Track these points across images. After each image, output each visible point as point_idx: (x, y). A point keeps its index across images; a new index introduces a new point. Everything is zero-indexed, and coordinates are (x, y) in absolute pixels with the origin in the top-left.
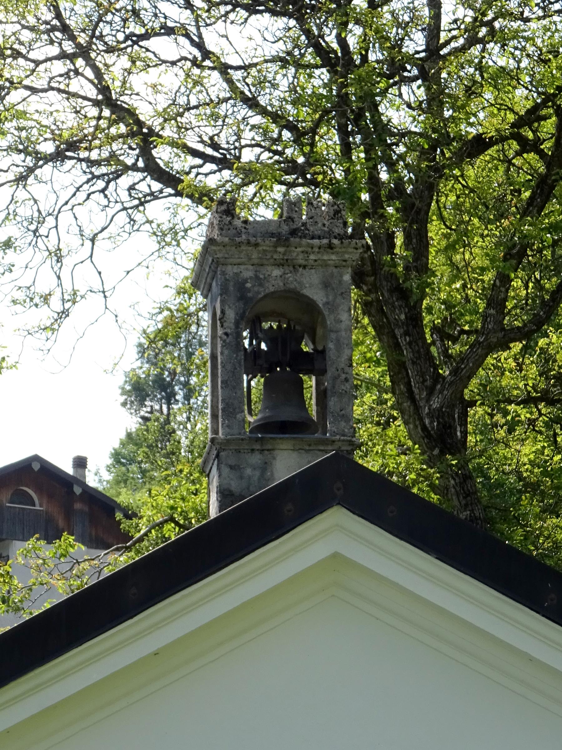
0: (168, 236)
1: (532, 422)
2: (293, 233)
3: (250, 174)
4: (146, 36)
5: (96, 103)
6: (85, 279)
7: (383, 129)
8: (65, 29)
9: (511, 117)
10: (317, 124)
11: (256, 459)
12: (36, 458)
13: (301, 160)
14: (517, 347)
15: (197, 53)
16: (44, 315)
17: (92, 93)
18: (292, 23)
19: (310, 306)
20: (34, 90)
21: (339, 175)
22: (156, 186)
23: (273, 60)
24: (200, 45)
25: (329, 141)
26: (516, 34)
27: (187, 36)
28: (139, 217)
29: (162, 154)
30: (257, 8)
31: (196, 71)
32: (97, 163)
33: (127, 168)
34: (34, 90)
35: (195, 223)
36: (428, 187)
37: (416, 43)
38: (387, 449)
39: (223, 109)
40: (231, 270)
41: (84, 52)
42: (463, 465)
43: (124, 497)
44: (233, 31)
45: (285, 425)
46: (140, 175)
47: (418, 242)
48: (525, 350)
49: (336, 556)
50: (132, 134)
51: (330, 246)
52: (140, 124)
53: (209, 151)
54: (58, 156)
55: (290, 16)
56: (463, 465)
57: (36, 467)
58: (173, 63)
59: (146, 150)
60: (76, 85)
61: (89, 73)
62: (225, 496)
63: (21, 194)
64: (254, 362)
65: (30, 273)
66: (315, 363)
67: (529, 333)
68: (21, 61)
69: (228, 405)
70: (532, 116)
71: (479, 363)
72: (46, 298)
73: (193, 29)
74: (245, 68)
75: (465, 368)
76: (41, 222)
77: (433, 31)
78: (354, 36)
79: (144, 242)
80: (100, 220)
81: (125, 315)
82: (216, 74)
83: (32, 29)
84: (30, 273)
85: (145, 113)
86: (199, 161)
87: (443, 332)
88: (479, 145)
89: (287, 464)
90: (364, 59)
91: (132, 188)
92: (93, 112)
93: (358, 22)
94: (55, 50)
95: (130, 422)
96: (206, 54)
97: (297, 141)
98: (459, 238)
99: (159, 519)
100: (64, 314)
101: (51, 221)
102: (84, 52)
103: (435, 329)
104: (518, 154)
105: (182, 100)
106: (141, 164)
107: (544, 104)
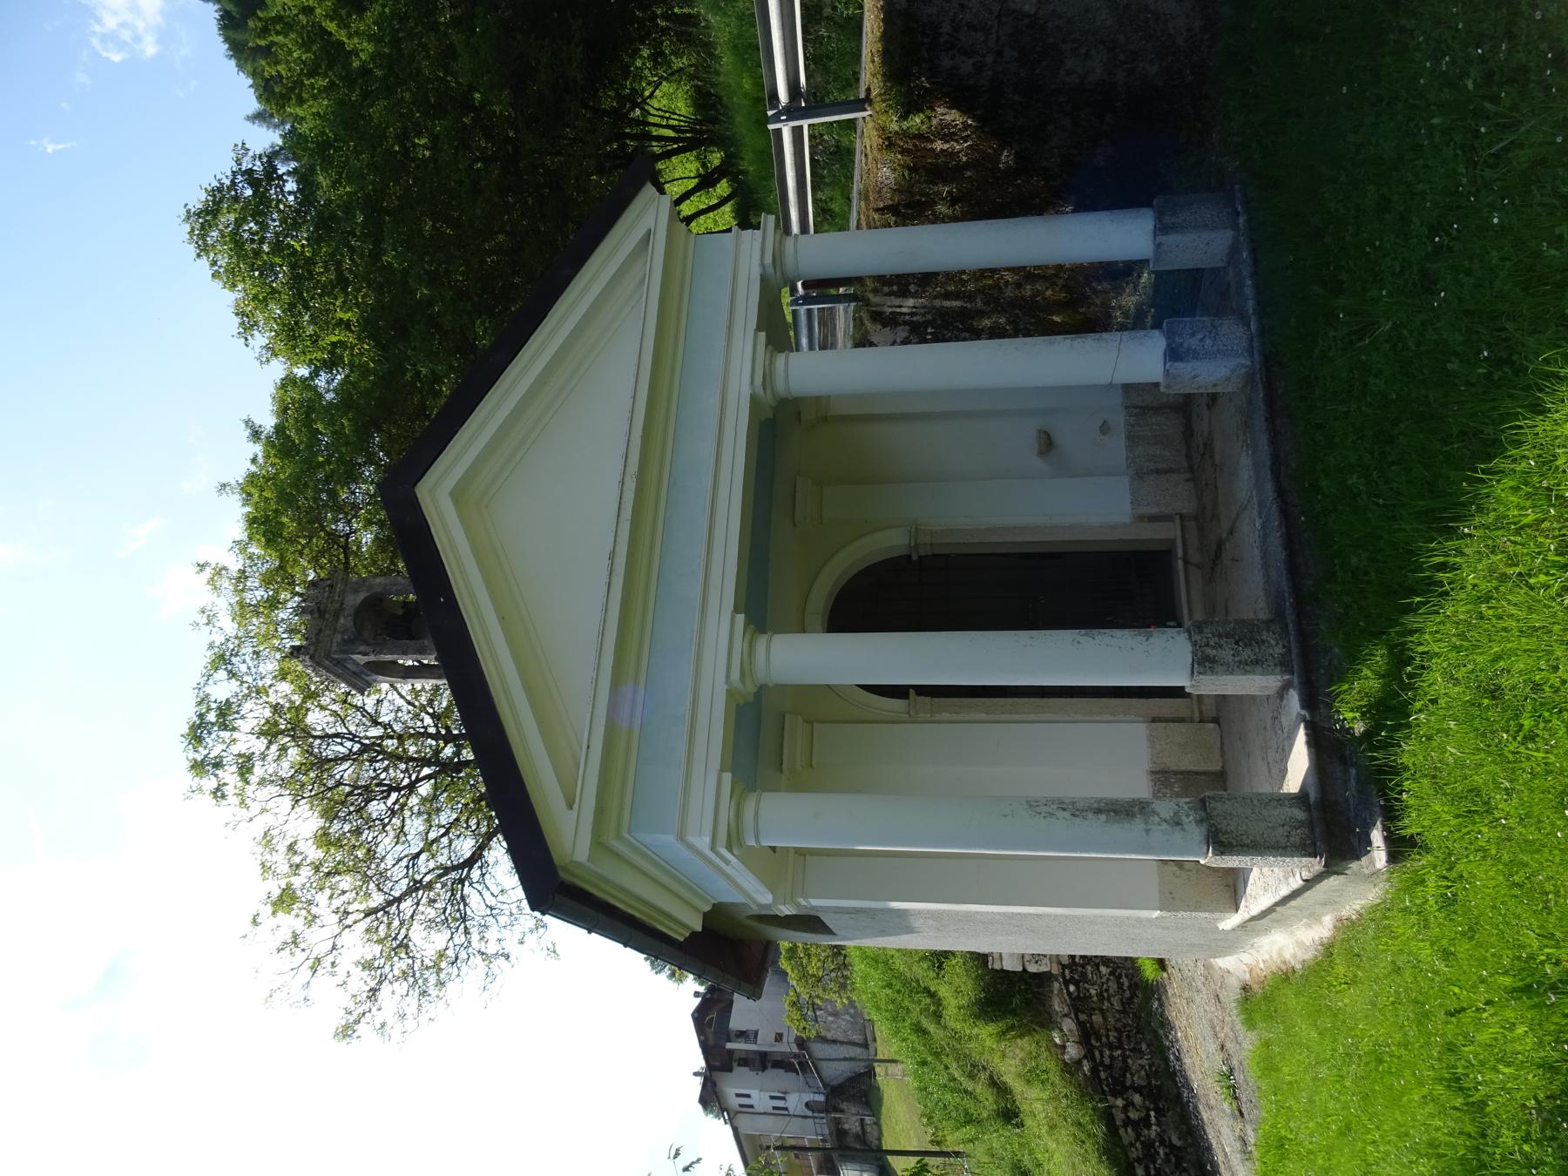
49: (451, 494)
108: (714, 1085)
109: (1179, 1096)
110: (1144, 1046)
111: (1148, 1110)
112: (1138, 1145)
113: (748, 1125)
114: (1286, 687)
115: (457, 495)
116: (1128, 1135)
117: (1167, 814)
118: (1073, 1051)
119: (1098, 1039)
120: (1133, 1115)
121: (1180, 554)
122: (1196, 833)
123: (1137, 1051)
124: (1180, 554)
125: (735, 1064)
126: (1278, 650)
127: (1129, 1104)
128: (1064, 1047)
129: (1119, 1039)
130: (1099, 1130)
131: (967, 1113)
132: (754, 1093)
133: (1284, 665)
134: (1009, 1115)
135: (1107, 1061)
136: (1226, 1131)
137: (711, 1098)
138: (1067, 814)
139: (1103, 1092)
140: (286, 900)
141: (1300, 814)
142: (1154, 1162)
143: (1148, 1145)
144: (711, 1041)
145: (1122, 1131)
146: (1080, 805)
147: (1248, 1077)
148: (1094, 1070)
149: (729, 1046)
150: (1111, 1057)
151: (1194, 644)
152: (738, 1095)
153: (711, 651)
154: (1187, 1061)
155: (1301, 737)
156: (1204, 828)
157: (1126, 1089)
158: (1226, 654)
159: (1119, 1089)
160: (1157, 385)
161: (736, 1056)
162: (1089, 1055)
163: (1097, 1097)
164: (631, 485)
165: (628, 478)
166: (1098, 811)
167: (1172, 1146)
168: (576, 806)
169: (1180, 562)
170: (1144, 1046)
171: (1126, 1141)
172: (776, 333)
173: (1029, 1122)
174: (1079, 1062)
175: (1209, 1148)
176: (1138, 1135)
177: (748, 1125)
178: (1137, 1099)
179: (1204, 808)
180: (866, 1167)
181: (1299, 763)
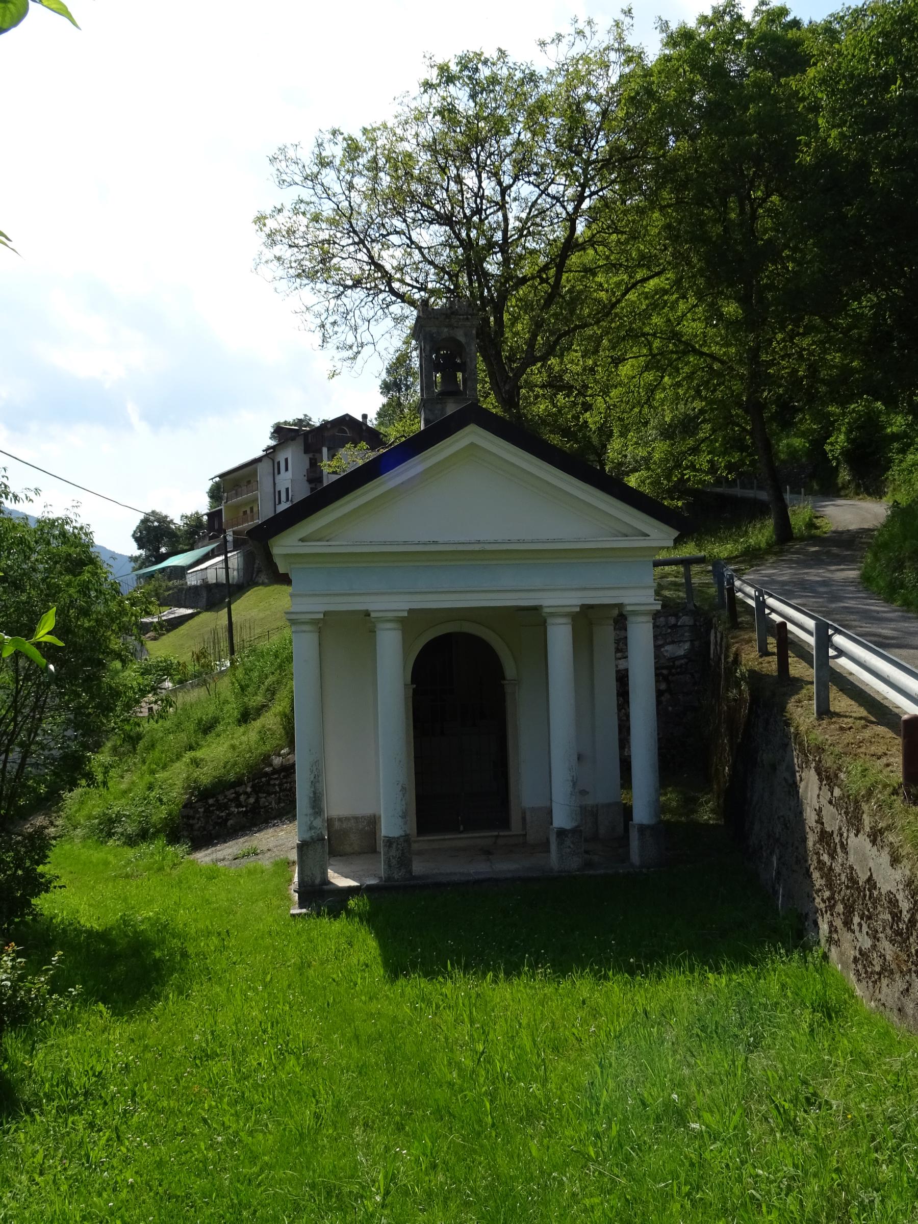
0: (399, 320)
1: (543, 395)
2: (452, 313)
3: (433, 292)
4: (388, 234)
5: (367, 263)
6: (366, 338)
7: (486, 274)
8: (355, 232)
9: (537, 268)
10: (459, 271)
11: (439, 406)
12: (347, 415)
13: (452, 287)
14: (539, 364)
15: (408, 242)
16: (350, 353)
17: (366, 259)
18: (448, 228)
19: (459, 344)
20: (343, 258)
21: (468, 293)
22: (394, 298)
23: (441, 245)
24: (410, 238)
25: (464, 279)
26: (539, 233)
27: (404, 234)
28: (386, 311)
29: (396, 285)
30: (62, 644)
31: (409, 250)
32: (370, 289)
33: (381, 291)
34: (343, 258)
35: (412, 313)
36: (504, 296)
37: (498, 236)
38: (491, 404)
39: (420, 265)
40: (428, 329)
41: (362, 242)
42: (518, 412)
43: (382, 430)
44: (423, 232)
45: (450, 392)
46: (386, 294)
47: (499, 321)
48: (542, 366)
49: (472, 444)
50: (383, 277)
51: (467, 319)
52: (387, 272)
53: (415, 284)
54: (355, 286)
55: (447, 225)
56: (518, 412)
57: (347, 418)
58: (399, 246)
59: (389, 284)
60: (360, 256)
61: (365, 250)
62: (427, 421)
63: (339, 302)
64: (437, 367)
65: (344, 335)
66: (462, 368)
67: (544, 358)
68: (336, 246)
69: (427, 385)
70: (546, 268)
71: (524, 372)
72: (351, 347)
73: (407, 232)
74: (429, 248)
75: (521, 371)
76: (348, 314)
77: (505, 231)
78: (474, 234)
79: (389, 322)
80: (372, 313)
81: (383, 353)
82: (417, 251)
83: (341, 232)
84: (344, 335)
85: (388, 267)
86: (410, 288)
87: (511, 359)
88: (524, 280)
89: (451, 408)
90: (477, 243)
91: (384, 299)
92: (367, 267)
93: (475, 228)
94: (351, 241)
95: (384, 400)
96: (412, 242)
97: (450, 279)
98: (515, 319)
99: (398, 435)
100: (359, 352)
101: (351, 314)
102: (362, 242)
103: (506, 357)
104: (540, 284)
105: (403, 262)
106: (387, 289)
107: (551, 262)
108: (293, 439)
109: (255, 825)
110: (282, 805)
111: (246, 807)
112: (226, 800)
113: (264, 470)
114: (381, 878)
115: (472, 445)
116: (231, 794)
117: (315, 824)
118: (277, 761)
119: (285, 777)
120: (242, 798)
121: (501, 834)
122: (307, 836)
123: (279, 801)
124: (501, 834)
125: (311, 455)
126: (396, 877)
127: (248, 795)
128: (279, 755)
129: (285, 790)
130: (232, 777)
131: (248, 686)
132: (289, 475)
133: (389, 879)
134: (245, 717)
135: (272, 782)
136: (230, 851)
137: (280, 431)
138: (312, 779)
139: (254, 780)
140: (353, 150)
141: (317, 881)
142: (217, 810)
143: (225, 807)
144: (326, 434)
145: (232, 791)
146: (317, 785)
147: (250, 863)
148: (266, 774)
149: (325, 450)
150: (274, 785)
151: (398, 838)
152: (286, 460)
153: (389, 601)
154: (271, 830)
155: (353, 883)
156: (308, 840)
157: (257, 794)
158: (393, 852)
159: (257, 789)
160: (552, 824)
161: (317, 455)
162: (275, 771)
163: (250, 776)
164: (477, 547)
165: (482, 545)
166: (315, 793)
167: (227, 820)
168: (301, 543)
169: (496, 833)
170: (282, 805)
171: (227, 793)
172: (586, 619)
173: (242, 729)
174: (271, 765)
175: (225, 842)
176: (231, 800)
177: (264, 470)
178: (252, 800)
179: (319, 840)
180: (241, 574)
181: (342, 882)
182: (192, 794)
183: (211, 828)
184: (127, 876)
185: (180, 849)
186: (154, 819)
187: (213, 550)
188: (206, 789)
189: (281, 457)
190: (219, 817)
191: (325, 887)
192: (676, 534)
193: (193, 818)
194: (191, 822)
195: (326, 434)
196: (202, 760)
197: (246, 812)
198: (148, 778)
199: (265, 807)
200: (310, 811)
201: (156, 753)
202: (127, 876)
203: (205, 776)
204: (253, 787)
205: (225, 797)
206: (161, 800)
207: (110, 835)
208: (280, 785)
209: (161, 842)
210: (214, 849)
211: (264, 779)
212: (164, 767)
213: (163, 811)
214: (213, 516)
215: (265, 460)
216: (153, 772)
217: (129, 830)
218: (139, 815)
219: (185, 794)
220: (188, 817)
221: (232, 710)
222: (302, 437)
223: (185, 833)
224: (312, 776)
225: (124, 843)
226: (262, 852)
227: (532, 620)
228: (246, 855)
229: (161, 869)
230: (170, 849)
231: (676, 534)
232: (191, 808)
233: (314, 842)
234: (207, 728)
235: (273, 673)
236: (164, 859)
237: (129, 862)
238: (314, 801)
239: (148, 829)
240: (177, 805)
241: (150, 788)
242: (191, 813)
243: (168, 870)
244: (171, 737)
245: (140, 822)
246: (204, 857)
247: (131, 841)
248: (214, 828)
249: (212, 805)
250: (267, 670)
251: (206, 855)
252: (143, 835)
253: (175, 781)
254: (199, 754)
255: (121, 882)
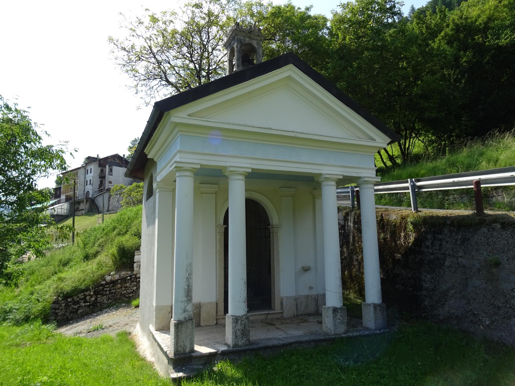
49: (290, 76)
108: (94, 161)
110: (110, 301)
111: (90, 302)
113: (81, 172)
115: (289, 78)
116: (81, 296)
117: (187, 308)
118: (108, 278)
119: (112, 286)
120: (88, 298)
121: (270, 312)
125: (101, 168)
126: (240, 343)
127: (91, 296)
128: (110, 275)
129: (112, 293)
130: (83, 287)
131: (87, 244)
132: (92, 174)
133: (235, 345)
134: (87, 258)
135: (105, 289)
136: (83, 327)
138: (187, 276)
139: (95, 288)
141: (187, 350)
142: (73, 304)
143: (78, 302)
144: (109, 160)
145: (82, 294)
146: (190, 280)
147: (102, 334)
148: (102, 285)
149: (107, 166)
150: (107, 291)
151: (242, 316)
153: (239, 161)
154: (106, 315)
156: (183, 320)
157: (96, 295)
159: (96, 293)
160: (325, 305)
161: (104, 168)
162: (107, 283)
163: (93, 286)
164: (293, 135)
166: (188, 286)
167: (78, 310)
170: (110, 301)
173: (85, 264)
174: (105, 280)
175: (77, 322)
176: (81, 299)
178: (93, 299)
181: (204, 350)
182: (59, 296)
183: (68, 314)
184: (17, 345)
185: (50, 327)
186: (34, 310)
187: (55, 202)
188: (67, 293)
189: (89, 168)
190: (73, 308)
191: (194, 354)
192: (389, 140)
193: (58, 309)
194: (57, 311)
195: (109, 160)
196: (65, 278)
197: (89, 305)
198: (30, 289)
199: (100, 302)
200: (186, 299)
201: (35, 276)
202: (17, 345)
203: (67, 287)
204: (94, 292)
205: (78, 297)
206: (38, 301)
207: (4, 320)
208: (110, 290)
209: (39, 323)
210: (71, 326)
211: (101, 288)
212: (40, 283)
213: (40, 306)
214: (56, 190)
215: (82, 168)
216: (33, 286)
217: (18, 317)
218: (25, 308)
219: (55, 296)
220: (55, 309)
221: (79, 254)
222: (98, 161)
223: (53, 318)
224: (187, 274)
225: (14, 324)
226: (106, 327)
227: (311, 183)
228: (96, 330)
229: (39, 339)
230: (43, 327)
231: (389, 140)
232: (57, 304)
233: (186, 321)
234: (65, 263)
235: (102, 237)
236: (40, 333)
237: (17, 335)
238: (188, 291)
239: (30, 317)
240: (49, 302)
241: (32, 294)
242: (57, 306)
243: (45, 340)
244: (44, 268)
245: (25, 312)
246: (68, 331)
247: (18, 323)
248: (70, 314)
249: (70, 302)
250: (98, 236)
251: (67, 330)
252: (27, 319)
253: (47, 291)
254: (63, 275)
255: (14, 350)
